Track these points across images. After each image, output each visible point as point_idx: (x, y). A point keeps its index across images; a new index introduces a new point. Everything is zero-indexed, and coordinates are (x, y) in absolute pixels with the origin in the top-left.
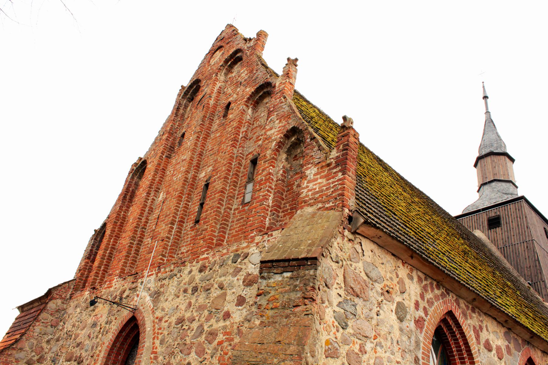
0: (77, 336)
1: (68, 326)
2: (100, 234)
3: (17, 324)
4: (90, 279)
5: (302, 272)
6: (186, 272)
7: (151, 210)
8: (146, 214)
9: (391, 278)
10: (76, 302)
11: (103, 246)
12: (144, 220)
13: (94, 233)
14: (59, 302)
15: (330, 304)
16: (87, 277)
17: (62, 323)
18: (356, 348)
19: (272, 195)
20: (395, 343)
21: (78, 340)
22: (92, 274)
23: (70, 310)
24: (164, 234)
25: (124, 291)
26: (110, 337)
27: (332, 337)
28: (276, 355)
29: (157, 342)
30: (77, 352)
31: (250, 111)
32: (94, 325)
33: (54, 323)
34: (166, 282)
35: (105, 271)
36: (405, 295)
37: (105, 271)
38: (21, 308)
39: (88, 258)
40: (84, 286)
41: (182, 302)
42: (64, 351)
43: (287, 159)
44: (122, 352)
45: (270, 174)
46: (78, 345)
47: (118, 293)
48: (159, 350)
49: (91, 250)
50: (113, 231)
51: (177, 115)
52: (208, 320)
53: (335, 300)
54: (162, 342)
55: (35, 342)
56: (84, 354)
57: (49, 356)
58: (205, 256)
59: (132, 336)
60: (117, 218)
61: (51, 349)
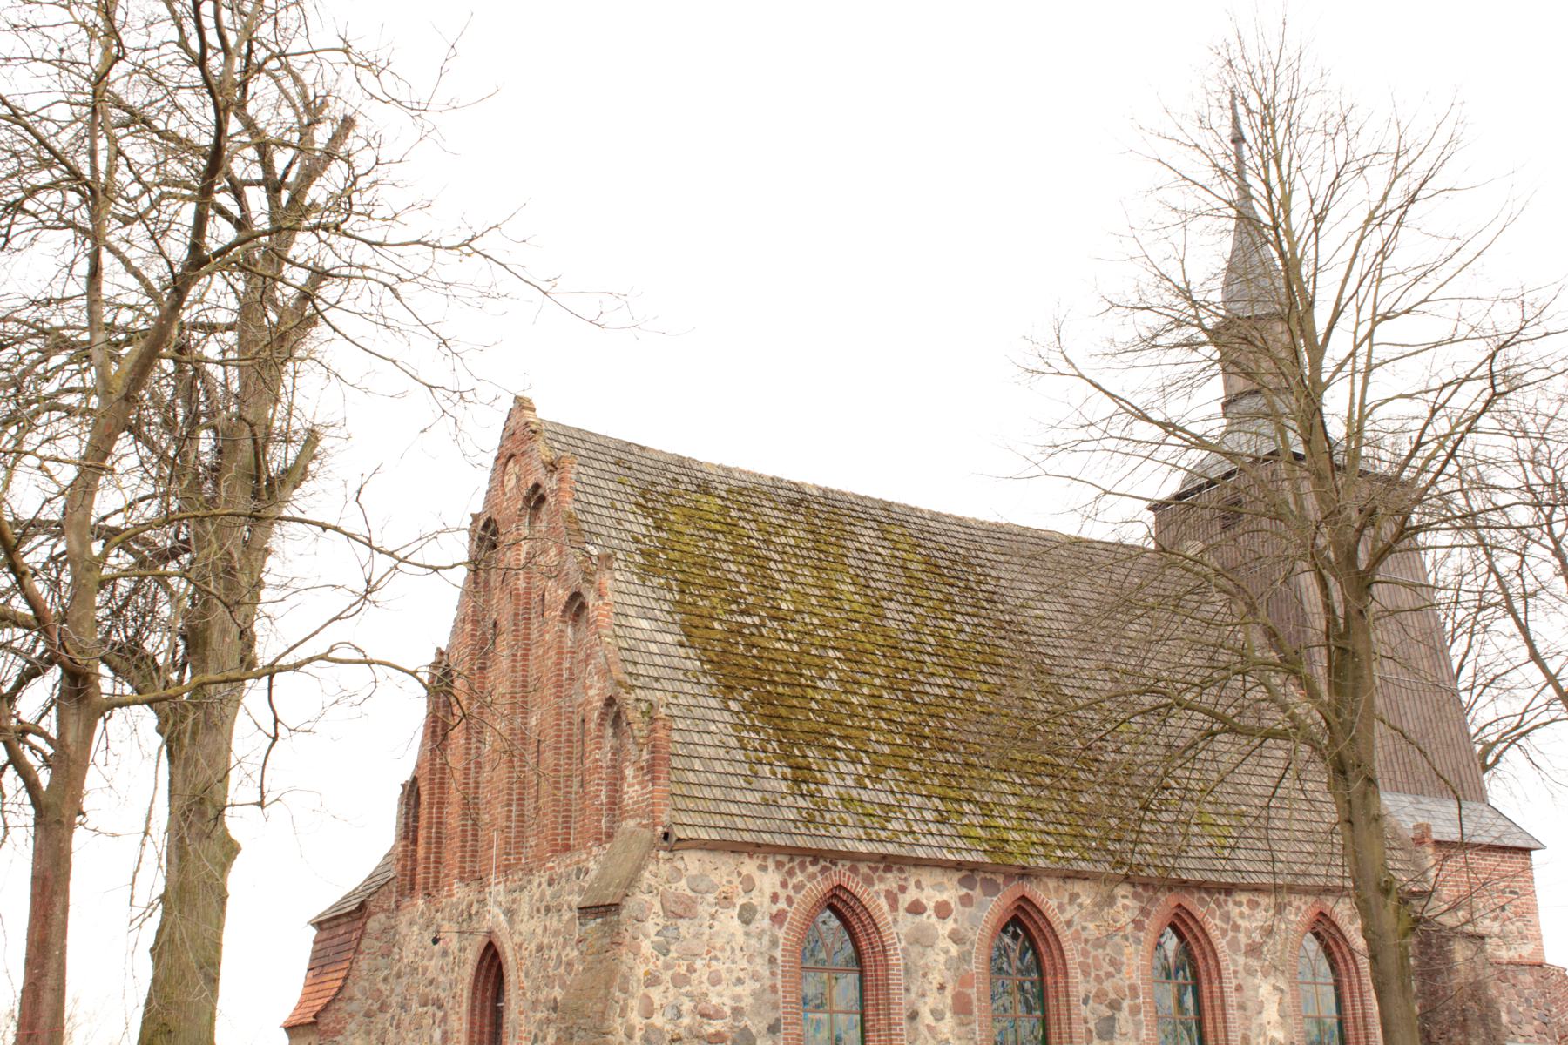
0: (425, 969)
1: (408, 956)
2: (411, 793)
3: (322, 953)
4: (420, 878)
6: (536, 884)
8: (472, 775)
10: (408, 916)
11: (423, 822)
12: (472, 785)
13: (400, 790)
14: (382, 917)
15: (647, 936)
16: (414, 869)
17: (396, 950)
18: (683, 970)
19: (604, 788)
20: (737, 951)
21: (429, 975)
22: (420, 869)
23: (403, 928)
25: (471, 905)
26: (469, 971)
27: (651, 966)
28: (590, 999)
29: (522, 975)
30: (433, 992)
31: (569, 631)
32: (445, 953)
33: (385, 951)
35: (437, 862)
36: (755, 892)
37: (437, 862)
38: (319, 925)
39: (406, 838)
40: (412, 889)
41: (536, 924)
42: (413, 992)
44: (490, 987)
45: (597, 760)
46: (431, 982)
47: (464, 906)
48: (525, 984)
49: (406, 824)
50: (431, 794)
52: (564, 948)
53: (652, 931)
55: (367, 984)
56: (442, 995)
57: (394, 1001)
59: (494, 971)
61: (392, 990)
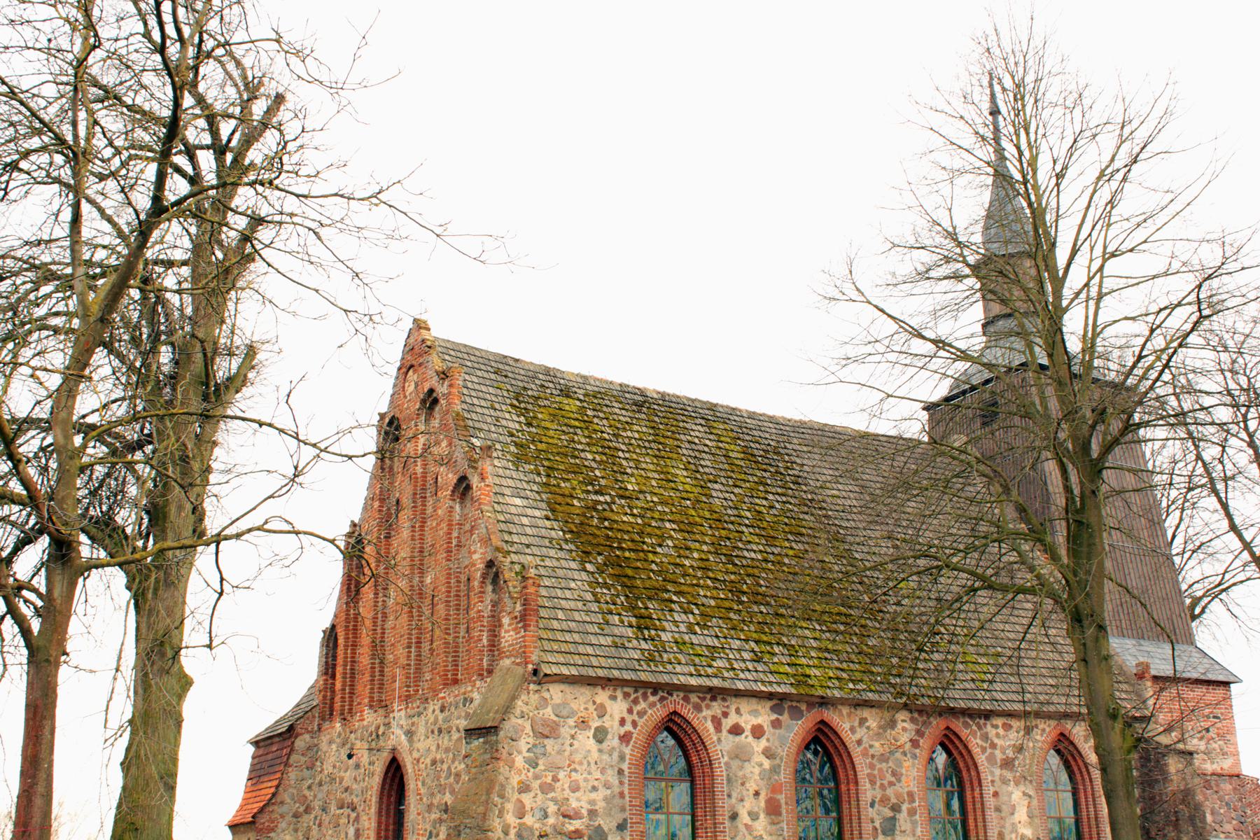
0: (342, 780)
2: (330, 637)
3: (258, 767)
4: (337, 705)
5: (489, 738)
7: (385, 616)
9: (586, 709)
11: (340, 660)
12: (379, 631)
14: (307, 736)
15: (520, 752)
17: (318, 764)
18: (549, 780)
19: (485, 634)
21: (345, 784)
22: (338, 698)
23: (324, 746)
24: (403, 661)
26: (377, 780)
27: (523, 777)
29: (420, 784)
30: (348, 798)
31: (457, 508)
34: (415, 719)
35: (351, 693)
36: (607, 717)
38: (256, 743)
39: (326, 674)
41: (431, 743)
43: (494, 591)
47: (373, 728)
48: (423, 791)
49: (327, 663)
50: (347, 639)
51: (383, 469)
52: (453, 762)
53: (524, 747)
54: (423, 784)
56: (355, 800)
58: (442, 695)
59: (397, 781)
60: (347, 620)
61: (315, 796)
